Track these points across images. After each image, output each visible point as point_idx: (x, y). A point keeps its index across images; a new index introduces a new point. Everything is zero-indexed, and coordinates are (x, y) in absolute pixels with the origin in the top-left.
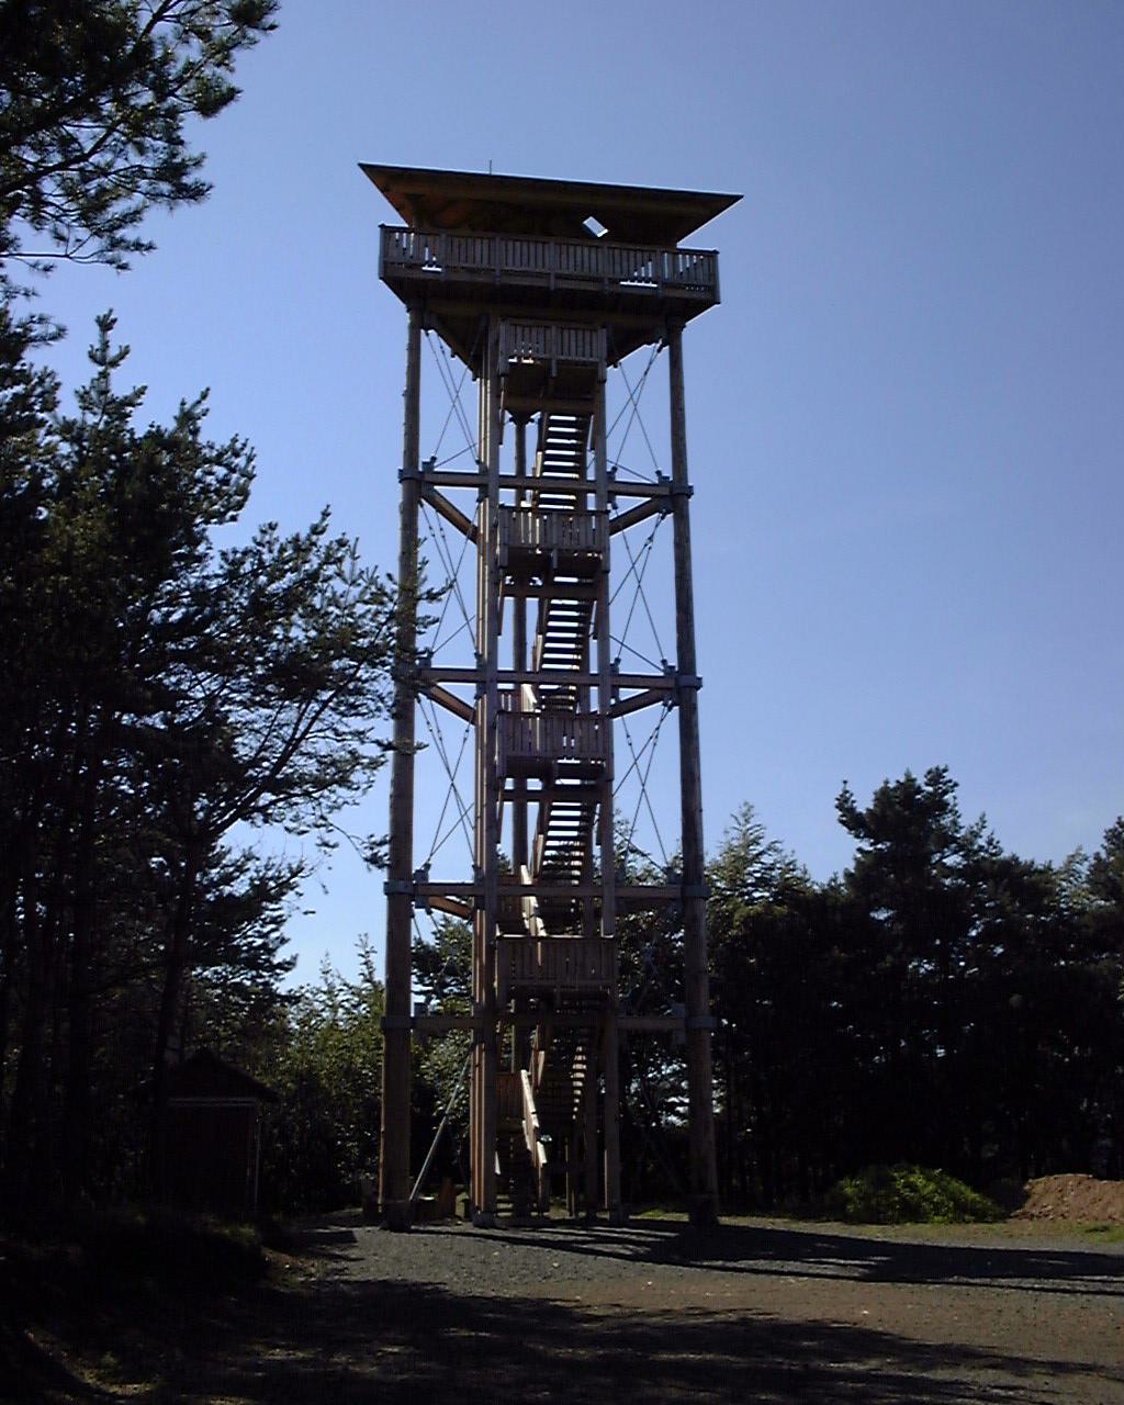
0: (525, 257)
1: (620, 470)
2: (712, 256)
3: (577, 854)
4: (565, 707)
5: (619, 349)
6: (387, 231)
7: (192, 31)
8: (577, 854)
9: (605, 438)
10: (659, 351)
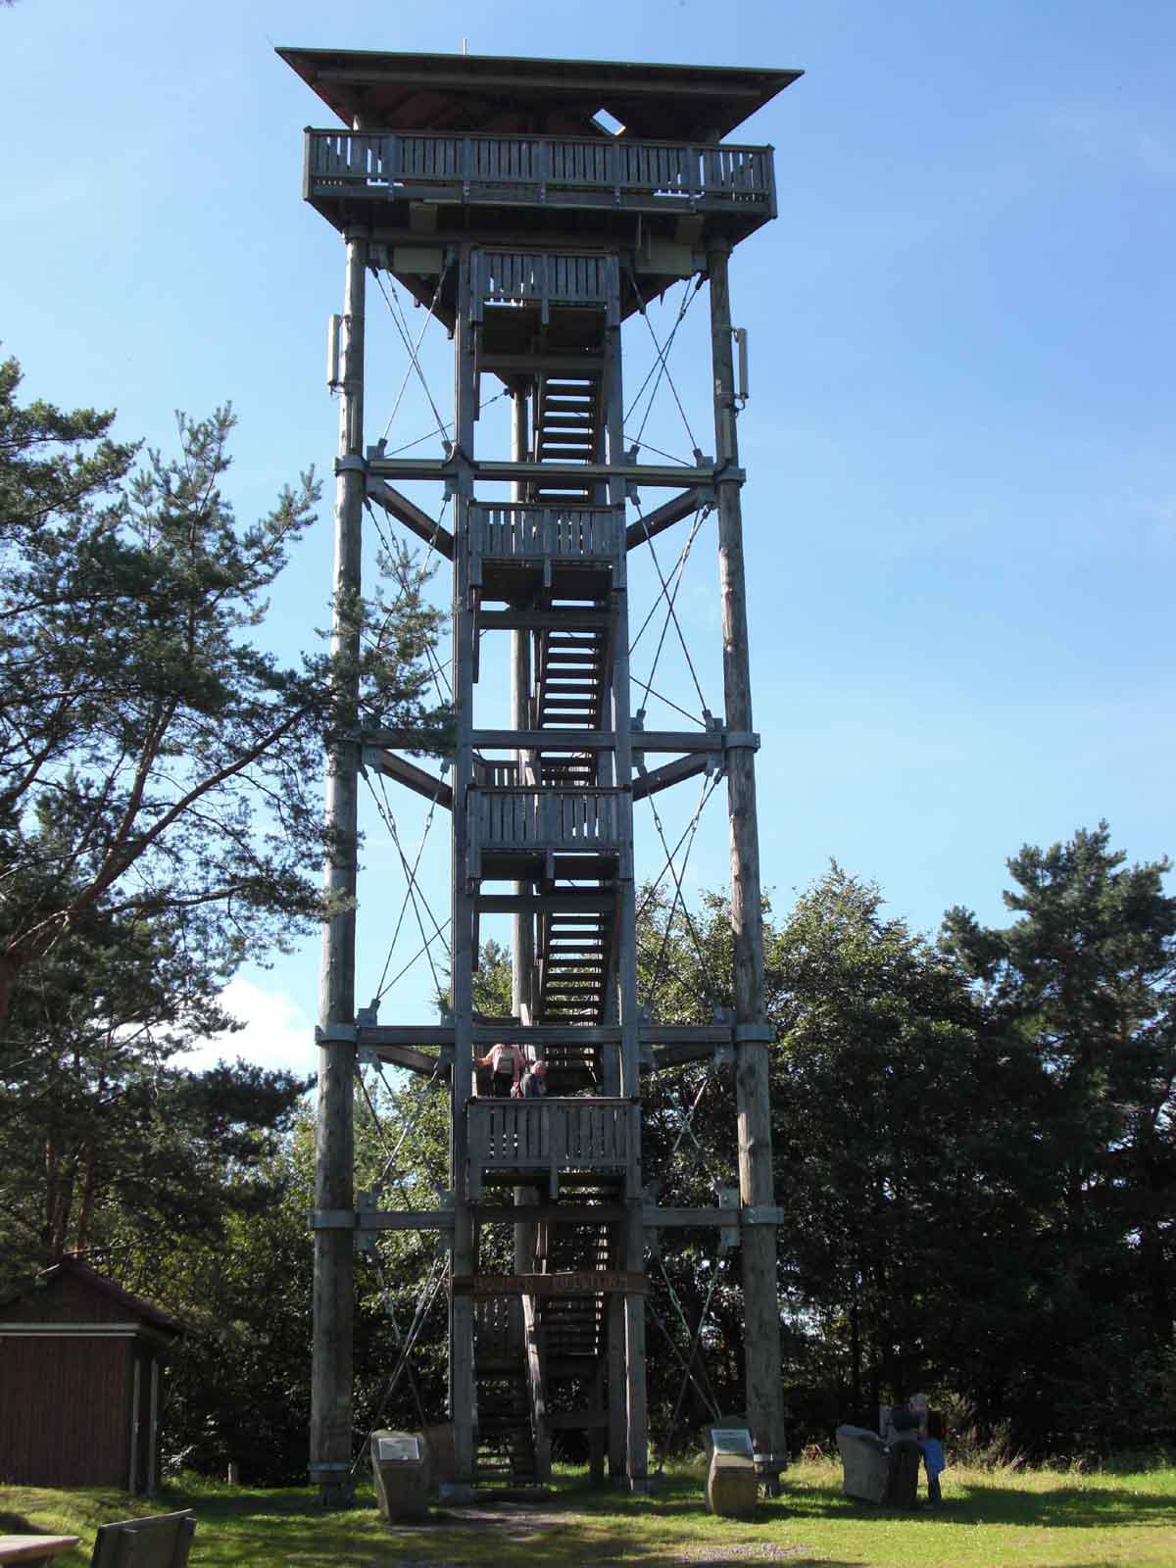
1: (642, 449)
2: (764, 154)
3: (581, 769)
4: (608, 1558)
5: (640, 290)
6: (315, 135)
7: (148, 689)
8: (581, 769)
9: (628, 654)
10: (698, 287)
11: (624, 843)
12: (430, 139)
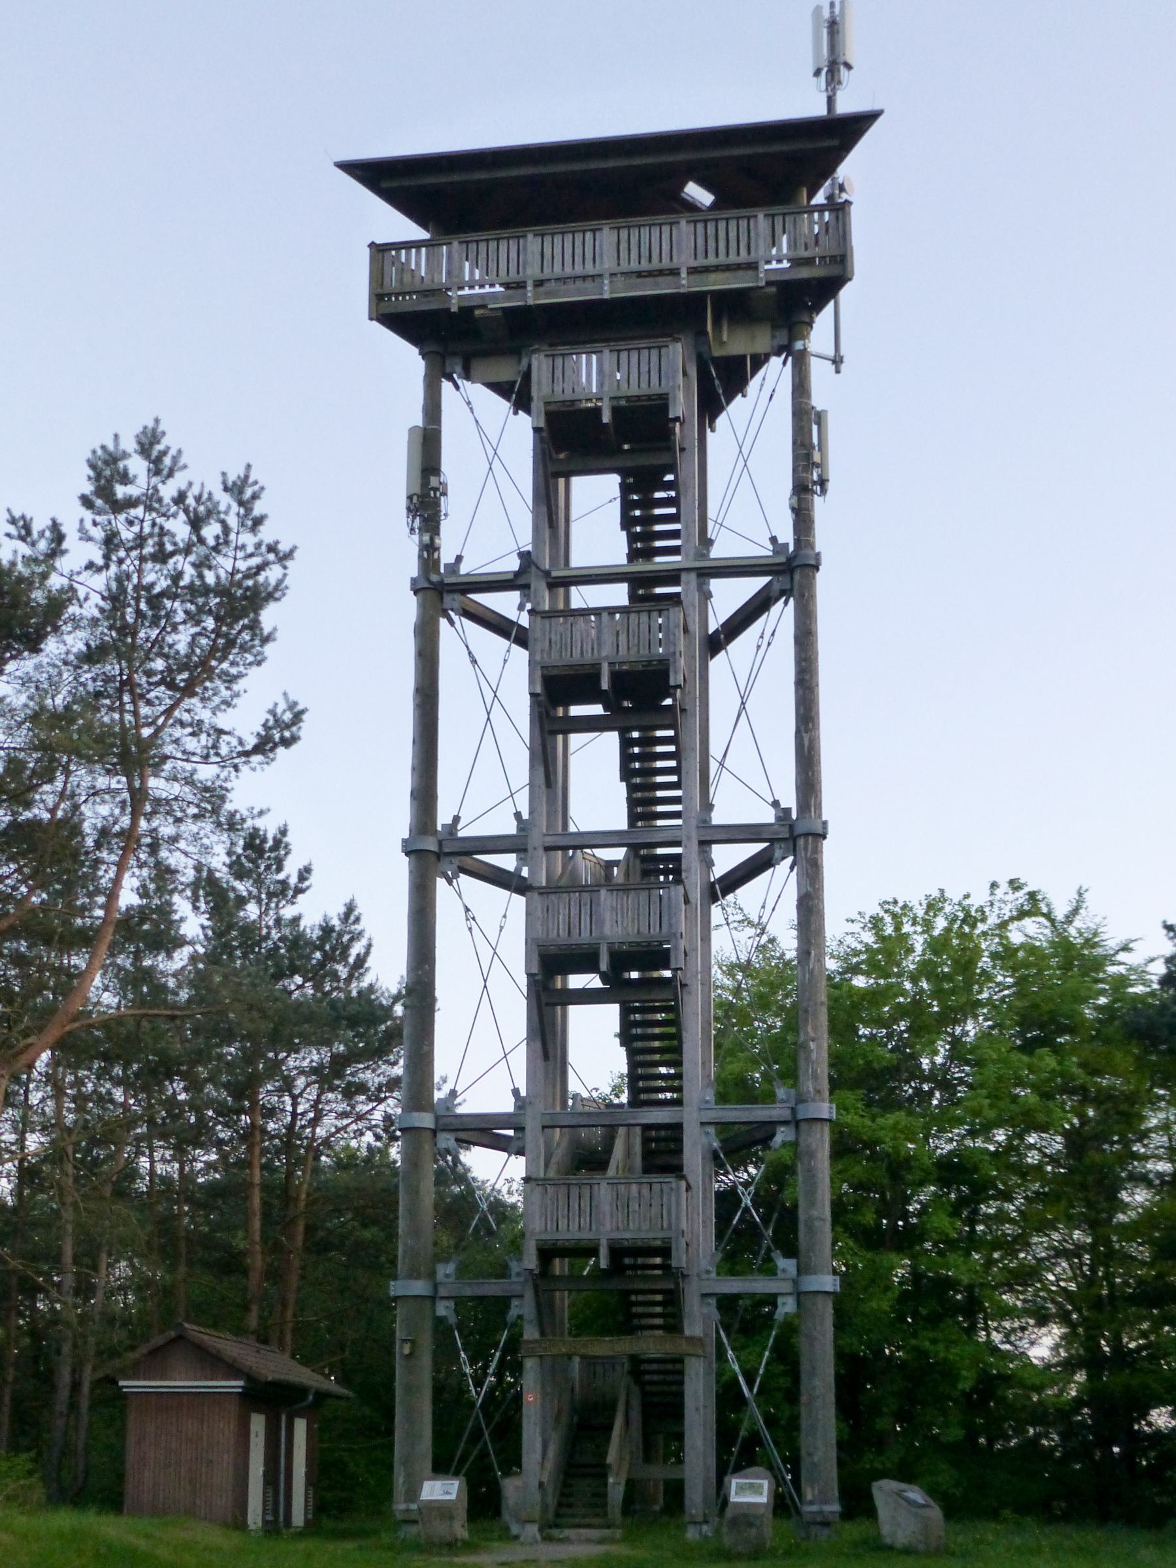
0: (733, 244)
6: (379, 251)
11: (675, 935)
12: (722, 219)
